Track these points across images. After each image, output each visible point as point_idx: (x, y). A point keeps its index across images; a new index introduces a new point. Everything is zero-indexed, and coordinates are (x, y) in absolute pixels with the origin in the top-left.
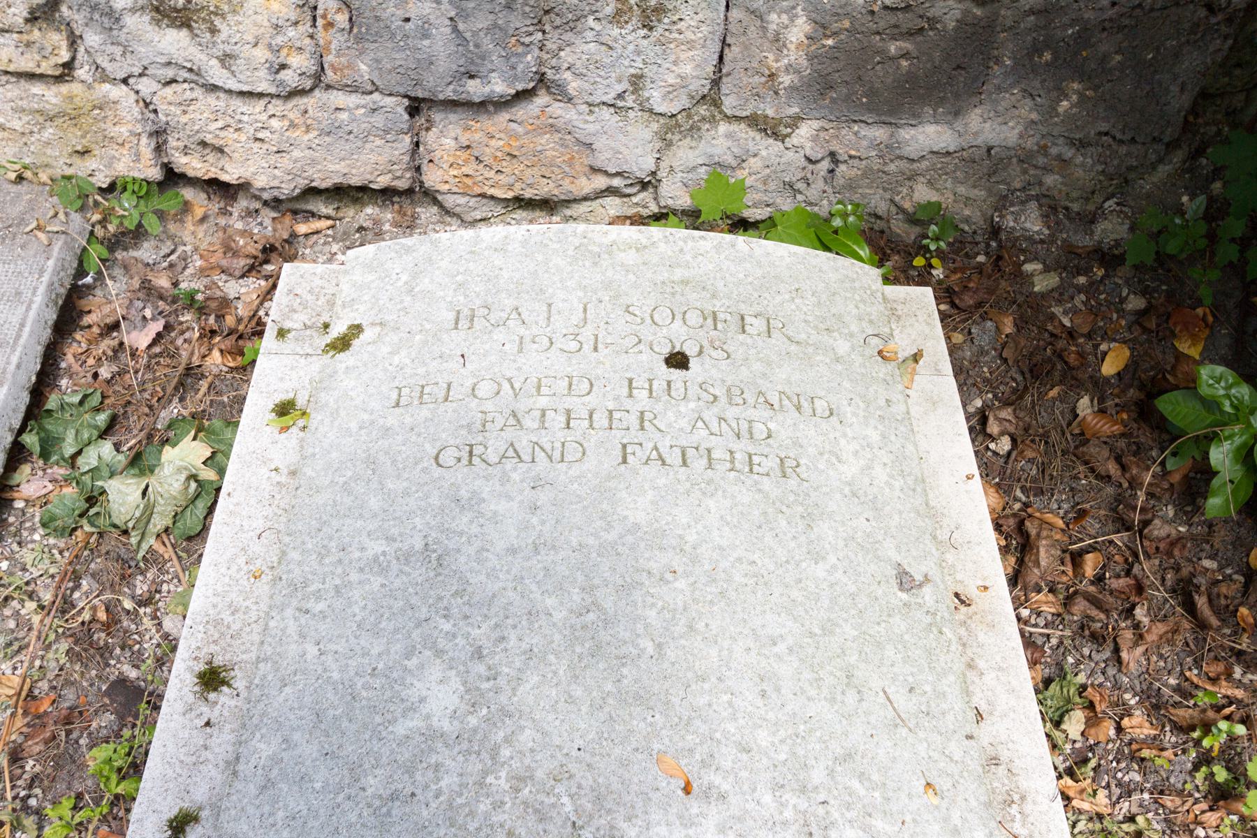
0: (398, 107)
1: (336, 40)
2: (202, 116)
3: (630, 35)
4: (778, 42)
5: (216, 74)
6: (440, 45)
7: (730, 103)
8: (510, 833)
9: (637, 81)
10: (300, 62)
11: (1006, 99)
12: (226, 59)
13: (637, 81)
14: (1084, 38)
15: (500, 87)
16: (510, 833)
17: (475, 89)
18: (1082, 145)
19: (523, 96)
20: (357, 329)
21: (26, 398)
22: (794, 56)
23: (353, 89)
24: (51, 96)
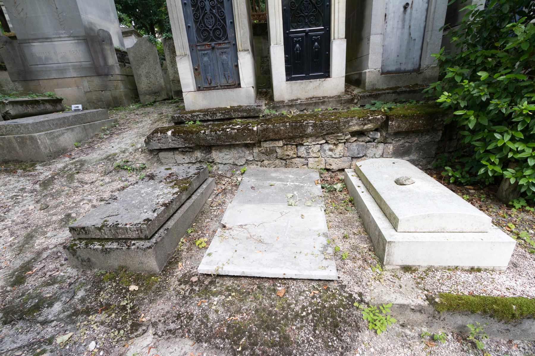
0: (350, 158)
1: (346, 151)
2: (331, 161)
3: (374, 149)
4: (389, 149)
5: (334, 156)
6: (356, 151)
7: (384, 156)
8: (1, 237)
9: (375, 154)
10: (342, 154)
11: (414, 154)
12: (335, 154)
13: (375, 154)
14: (421, 146)
15: (361, 155)
16: (1, 237)
17: (359, 156)
18: (424, 158)
19: (363, 156)
20: (245, 171)
21: (312, 96)
22: (391, 150)
23: (346, 157)
24: (317, 159)
